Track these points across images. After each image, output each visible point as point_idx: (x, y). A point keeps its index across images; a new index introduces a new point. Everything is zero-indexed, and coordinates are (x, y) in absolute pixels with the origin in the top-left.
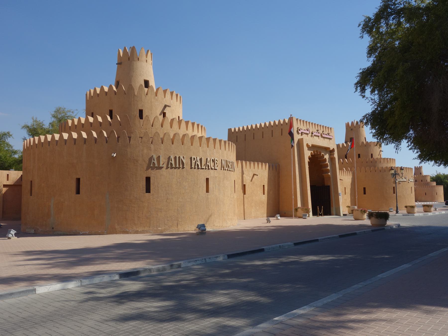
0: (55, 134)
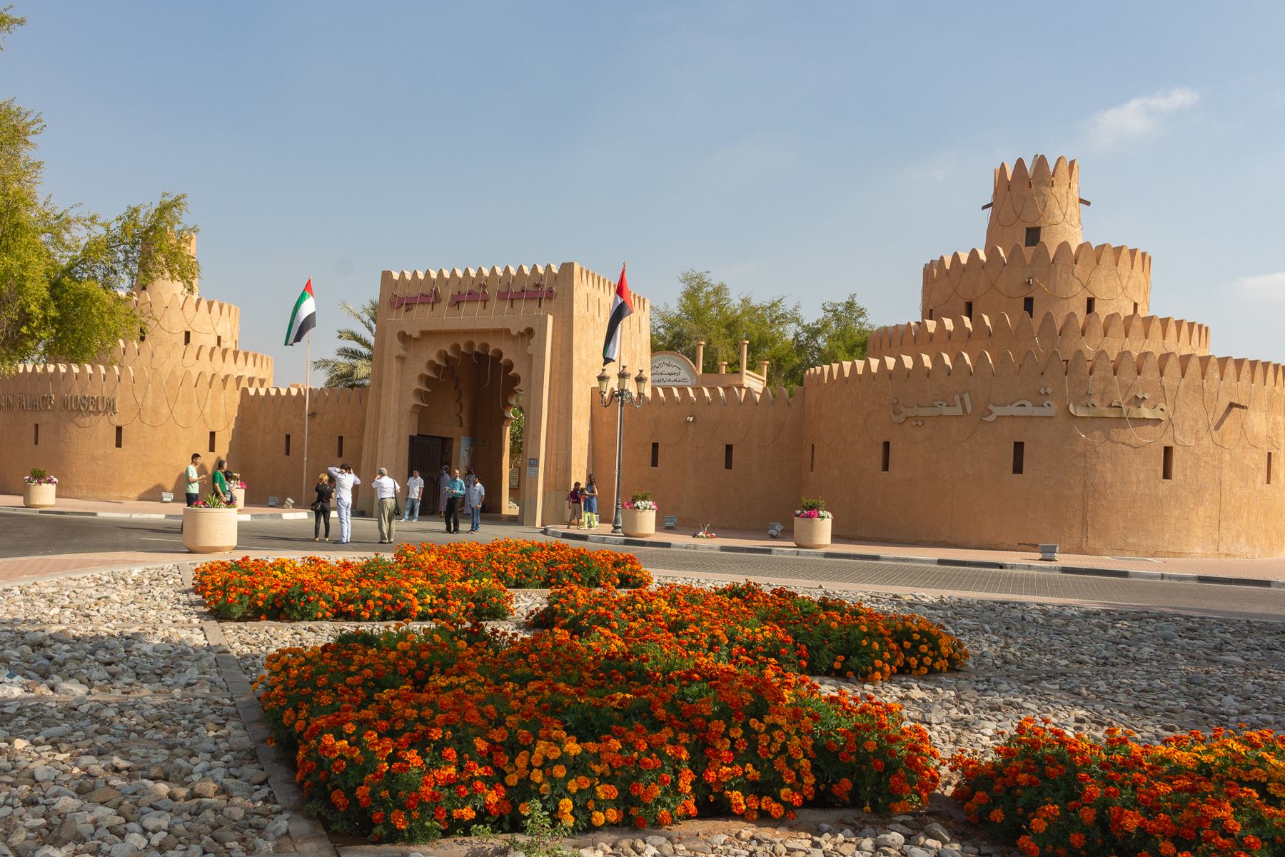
0: (871, 359)
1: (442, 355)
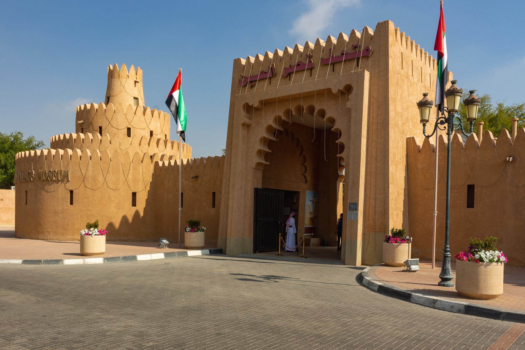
1: (278, 120)
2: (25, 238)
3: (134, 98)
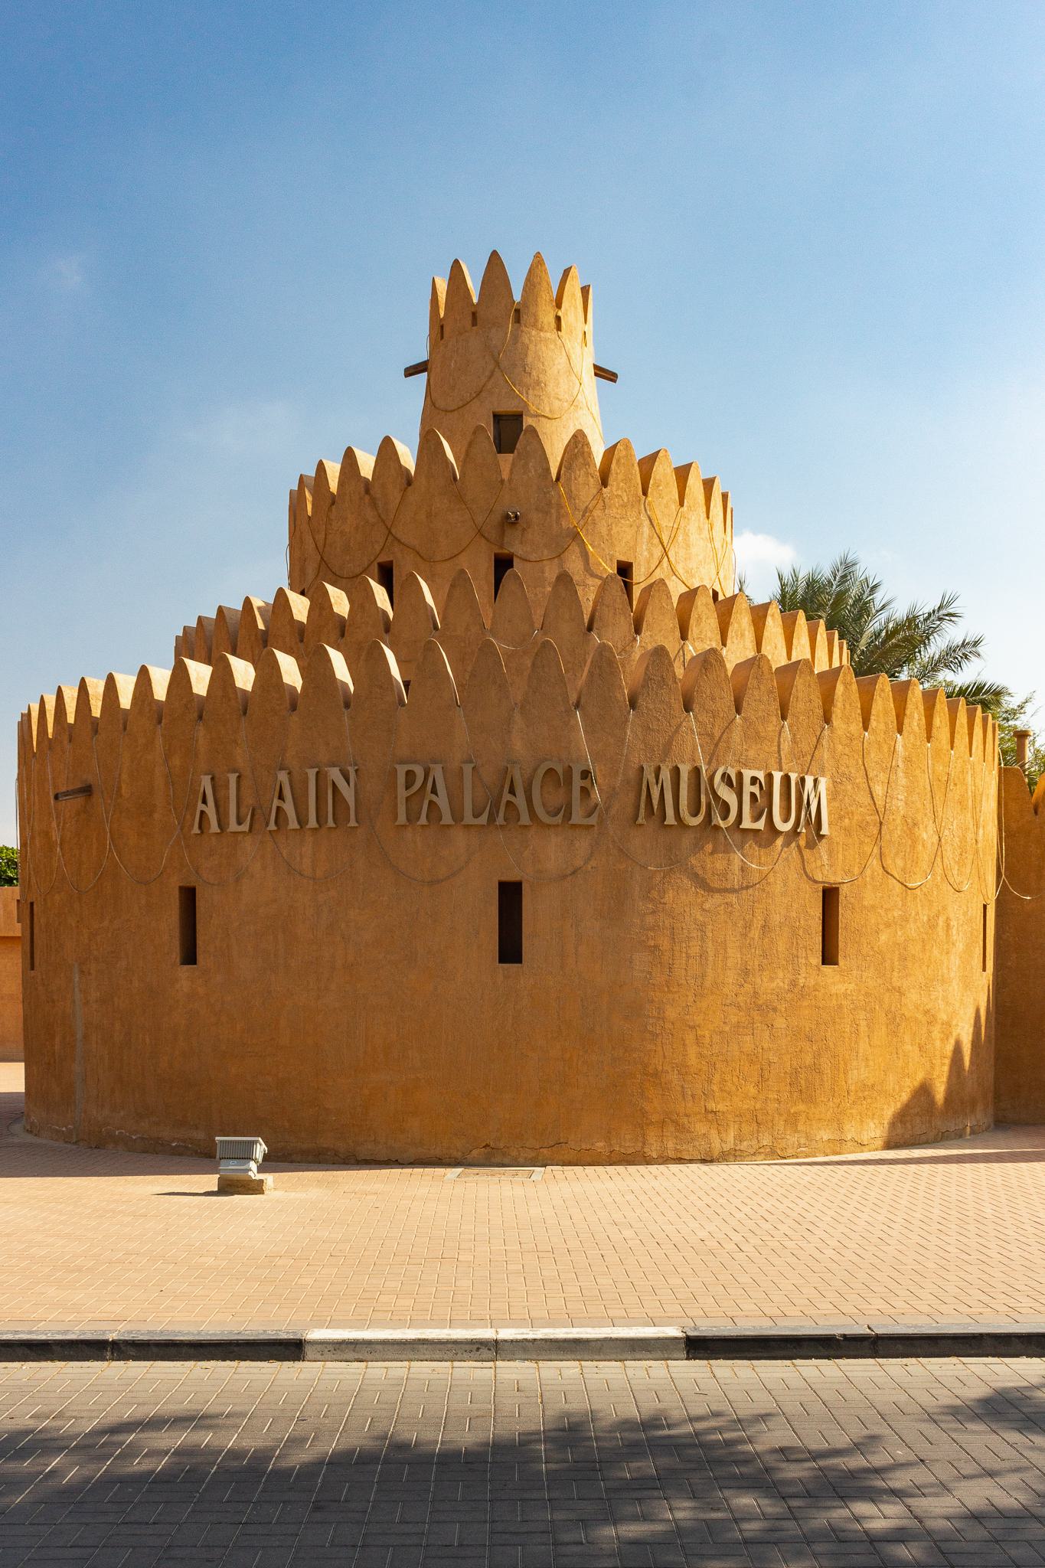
2: (498, 1160)
3: (596, 375)
